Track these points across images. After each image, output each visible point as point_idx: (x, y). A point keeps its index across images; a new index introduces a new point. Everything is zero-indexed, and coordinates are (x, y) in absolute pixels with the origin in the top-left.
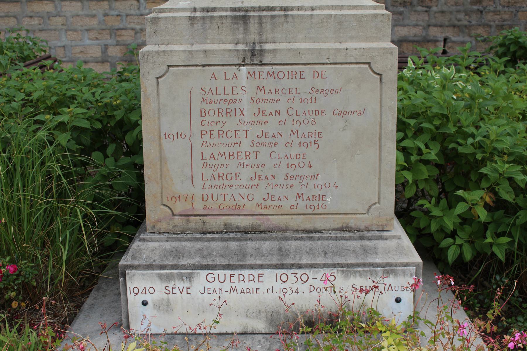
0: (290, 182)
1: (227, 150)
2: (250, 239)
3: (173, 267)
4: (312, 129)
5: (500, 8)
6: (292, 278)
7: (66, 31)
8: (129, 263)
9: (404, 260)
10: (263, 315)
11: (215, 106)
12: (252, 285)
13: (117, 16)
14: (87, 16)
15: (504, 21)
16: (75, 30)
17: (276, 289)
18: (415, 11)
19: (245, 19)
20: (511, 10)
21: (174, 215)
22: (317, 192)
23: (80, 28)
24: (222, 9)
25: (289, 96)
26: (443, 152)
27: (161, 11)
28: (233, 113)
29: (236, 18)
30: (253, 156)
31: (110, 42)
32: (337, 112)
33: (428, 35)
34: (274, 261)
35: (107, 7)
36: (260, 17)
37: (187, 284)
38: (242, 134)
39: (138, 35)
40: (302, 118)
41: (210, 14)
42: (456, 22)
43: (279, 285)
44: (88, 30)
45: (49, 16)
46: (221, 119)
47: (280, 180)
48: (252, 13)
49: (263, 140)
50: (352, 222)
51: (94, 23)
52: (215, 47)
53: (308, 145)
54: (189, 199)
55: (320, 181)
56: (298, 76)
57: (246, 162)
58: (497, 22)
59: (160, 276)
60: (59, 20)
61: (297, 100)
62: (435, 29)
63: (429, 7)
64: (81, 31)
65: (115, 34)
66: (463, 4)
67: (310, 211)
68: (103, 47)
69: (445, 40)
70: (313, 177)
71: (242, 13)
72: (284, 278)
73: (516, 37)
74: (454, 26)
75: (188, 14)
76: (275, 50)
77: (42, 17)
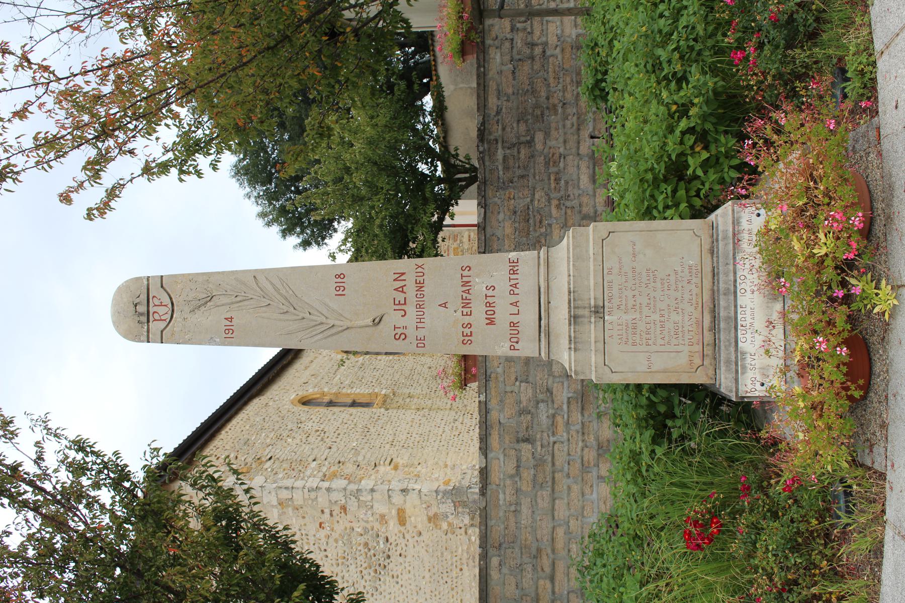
0: (680, 288)
1: (658, 329)
2: (719, 314)
3: (737, 364)
4: (644, 274)
5: (560, 86)
6: (743, 286)
7: (583, 517)
8: (734, 394)
9: (730, 212)
10: (770, 305)
11: (630, 336)
12: (748, 312)
13: (569, 464)
14: (569, 494)
15: (572, 81)
16: (583, 508)
17: (751, 296)
18: (564, 169)
19: (576, 317)
20: (561, 76)
21: (703, 365)
22: (687, 271)
23: (581, 503)
24: (570, 331)
25: (624, 290)
26: (666, 180)
27: (571, 370)
28: (635, 325)
29: (575, 323)
30: (662, 312)
31: (595, 473)
32: (633, 259)
33: (587, 154)
34: (732, 298)
35: (560, 474)
36: (575, 308)
37: (748, 355)
38: (648, 319)
39: (588, 444)
40: (637, 281)
41: (573, 339)
42: (575, 127)
43: (748, 294)
44: (583, 495)
45: (568, 532)
46: (638, 332)
47: (679, 295)
48: (572, 313)
49: (652, 306)
50: (706, 246)
51: (576, 488)
52: (593, 336)
53: (655, 277)
54: (692, 354)
55: (679, 269)
56: (611, 284)
57: (667, 316)
58: (574, 88)
59: (743, 373)
60: (572, 523)
61: (626, 284)
62: (581, 148)
63: (560, 155)
64: (583, 502)
65: (587, 467)
66: (557, 122)
67: (700, 275)
68: (600, 480)
69: (592, 137)
70: (676, 273)
71: (572, 319)
72: (743, 291)
73: (588, 90)
74: (579, 129)
75: (573, 352)
76: (595, 299)
77: (570, 539)
